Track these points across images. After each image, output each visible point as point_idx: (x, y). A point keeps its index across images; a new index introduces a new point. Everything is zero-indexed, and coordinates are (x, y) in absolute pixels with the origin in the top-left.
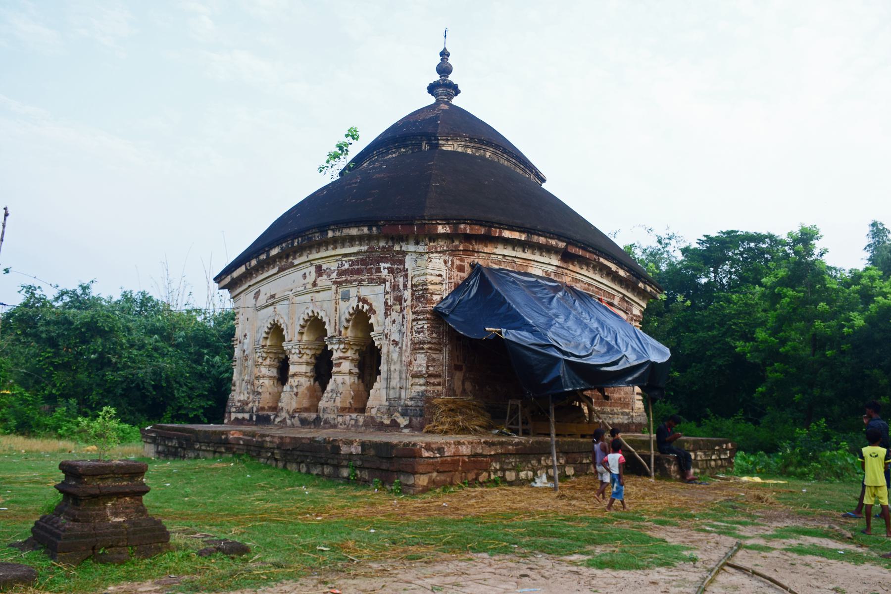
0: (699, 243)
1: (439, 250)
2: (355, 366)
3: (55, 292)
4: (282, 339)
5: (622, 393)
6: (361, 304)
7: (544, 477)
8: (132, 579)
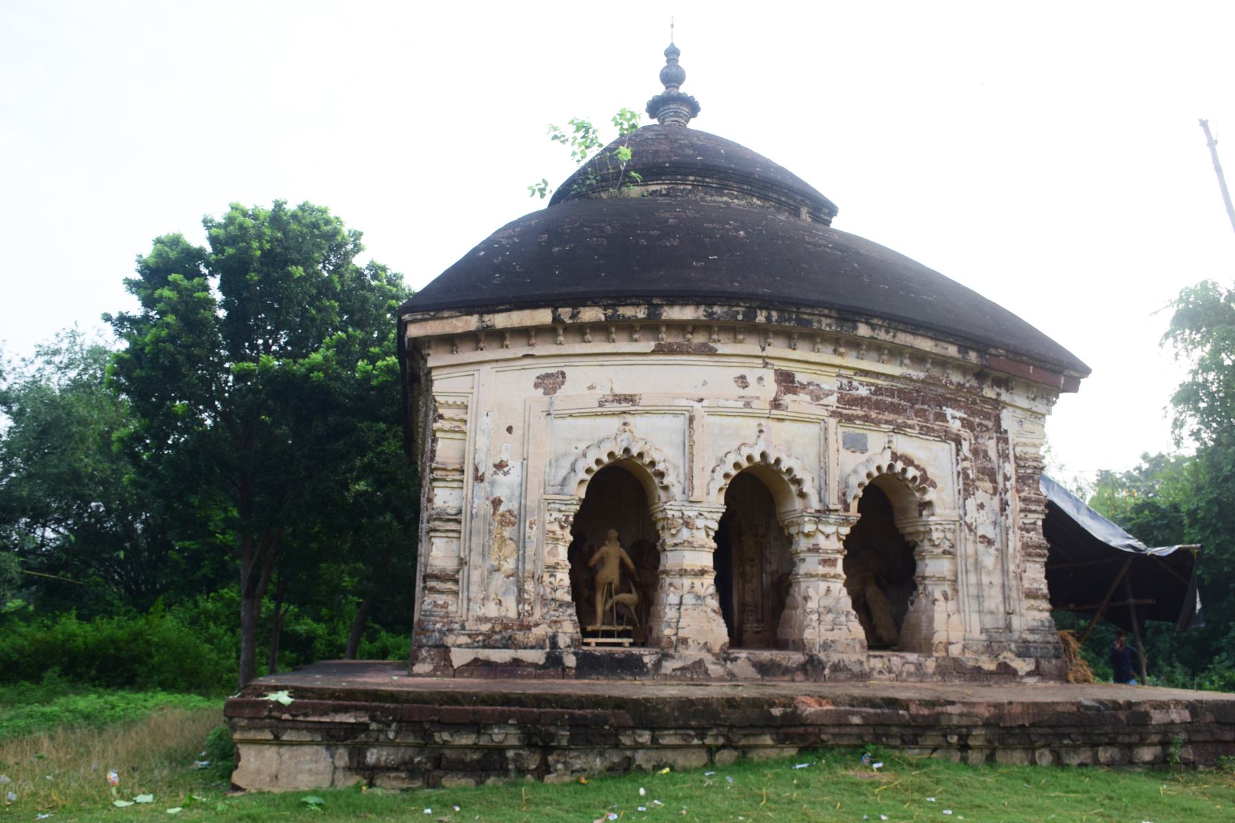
6: (899, 466)
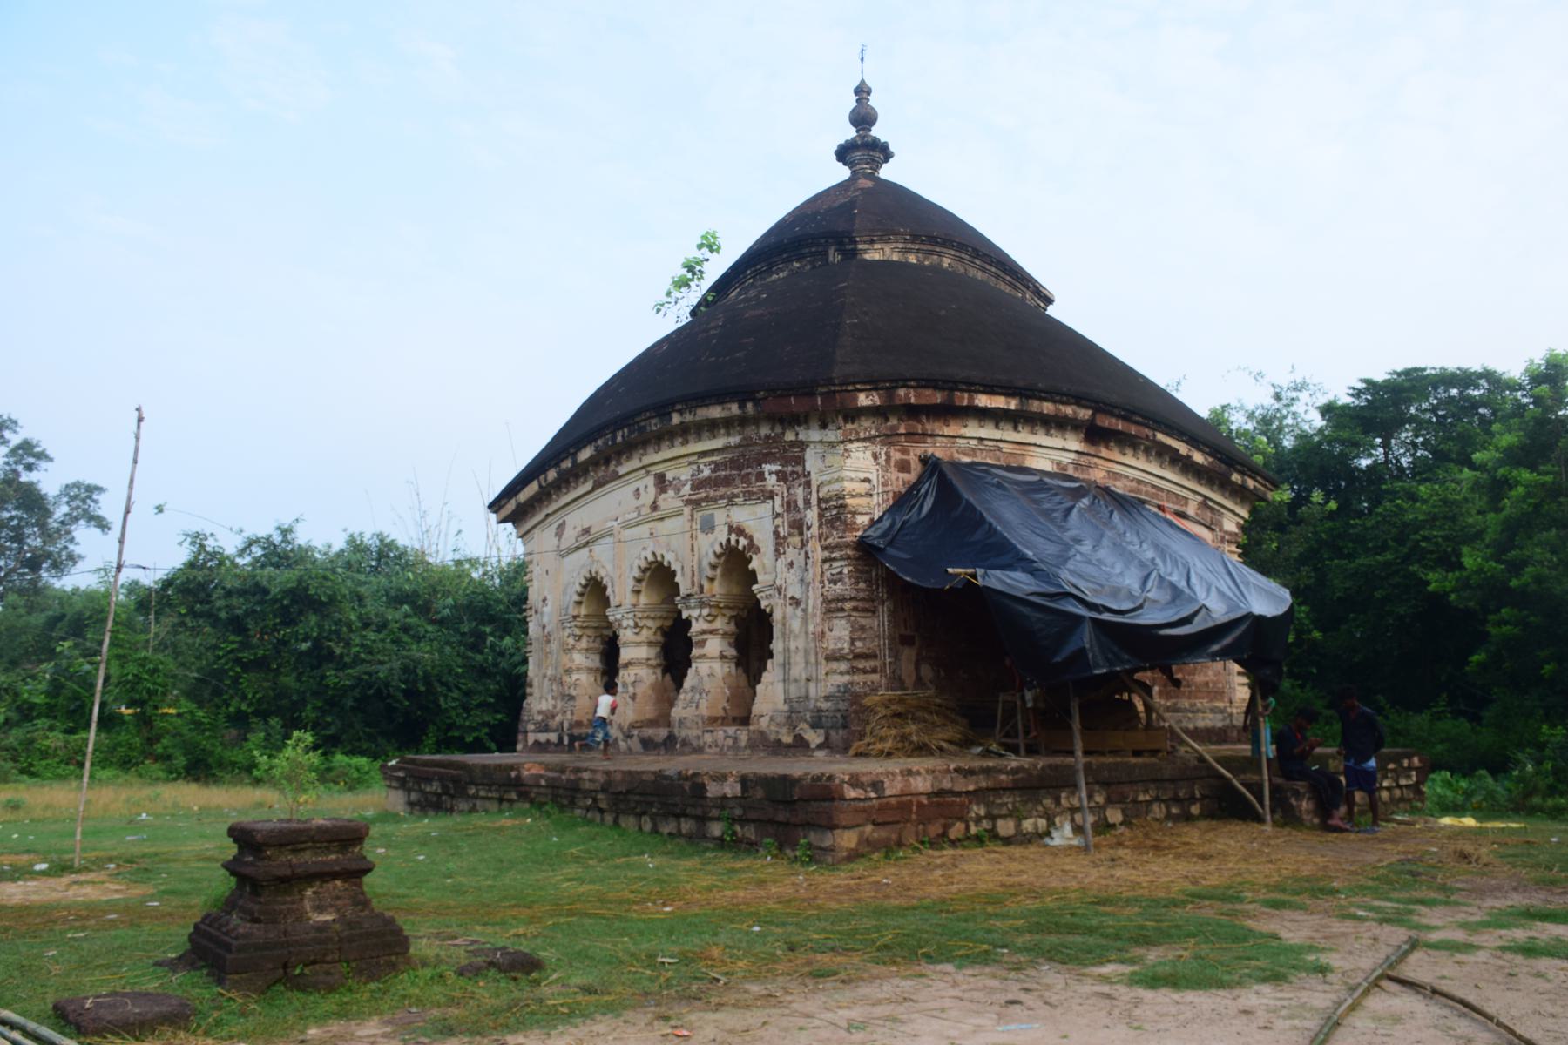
0: (1352, 395)
1: (862, 435)
2: (730, 645)
4: (605, 602)
5: (1210, 673)
6: (733, 537)
7: (1067, 829)
8: (346, 1016)
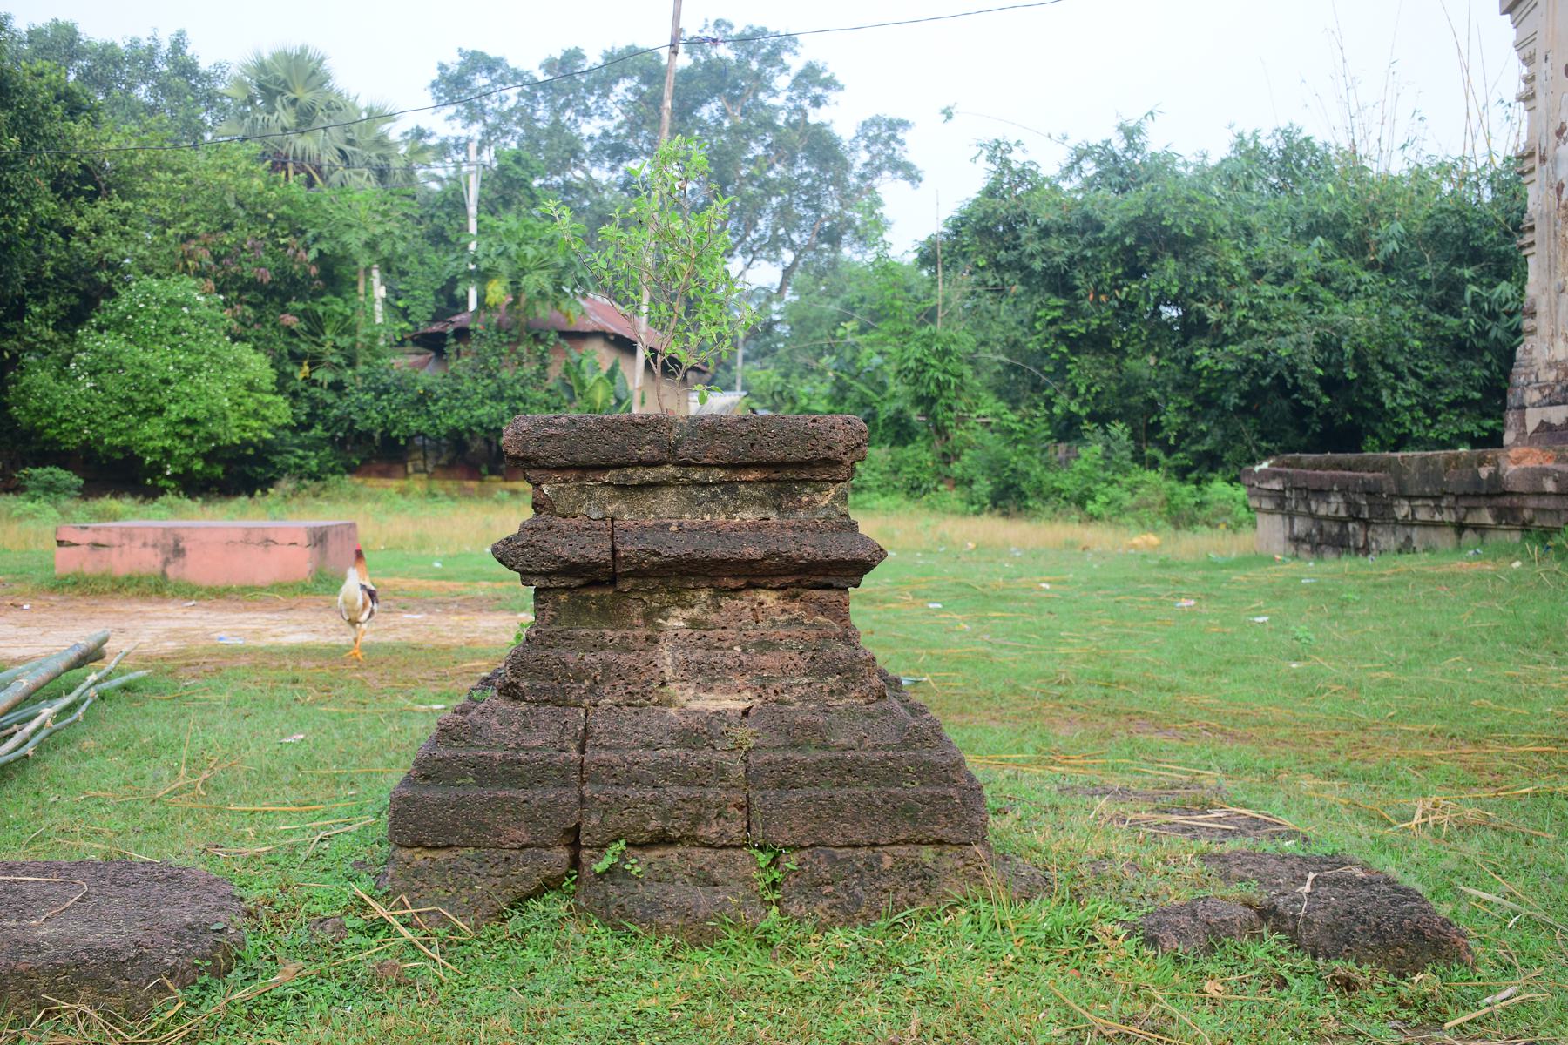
3: (1063, 156)
